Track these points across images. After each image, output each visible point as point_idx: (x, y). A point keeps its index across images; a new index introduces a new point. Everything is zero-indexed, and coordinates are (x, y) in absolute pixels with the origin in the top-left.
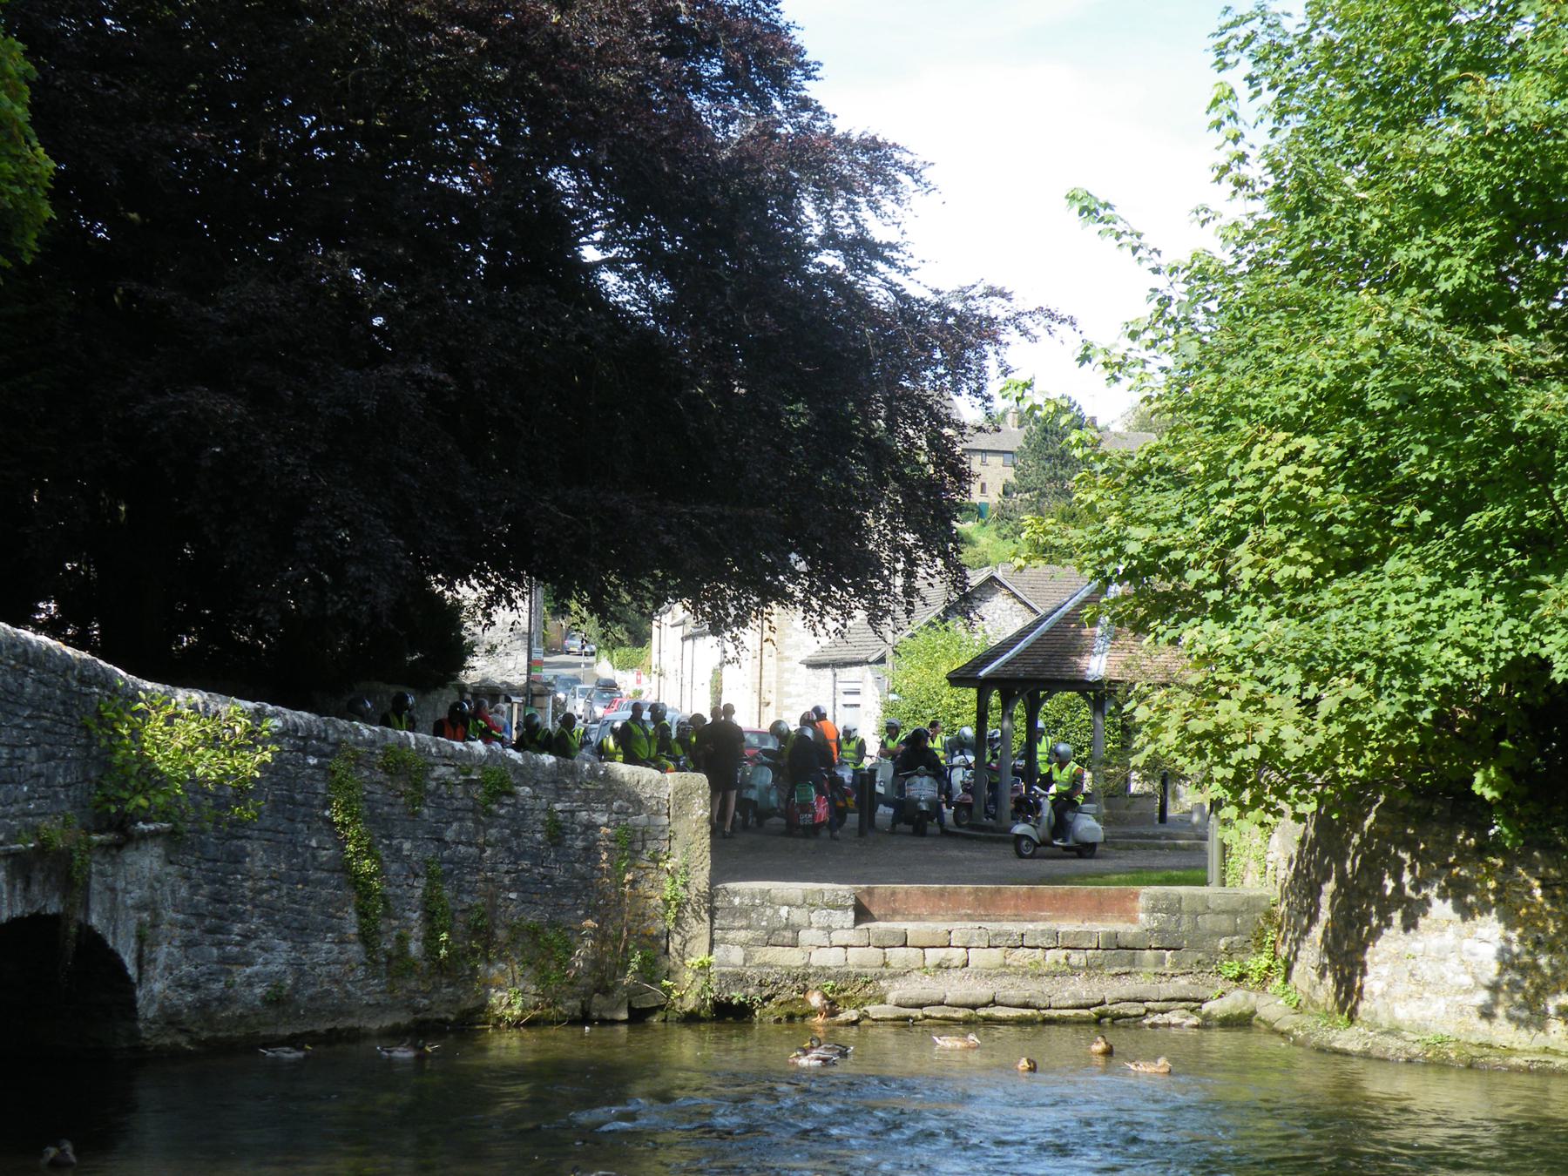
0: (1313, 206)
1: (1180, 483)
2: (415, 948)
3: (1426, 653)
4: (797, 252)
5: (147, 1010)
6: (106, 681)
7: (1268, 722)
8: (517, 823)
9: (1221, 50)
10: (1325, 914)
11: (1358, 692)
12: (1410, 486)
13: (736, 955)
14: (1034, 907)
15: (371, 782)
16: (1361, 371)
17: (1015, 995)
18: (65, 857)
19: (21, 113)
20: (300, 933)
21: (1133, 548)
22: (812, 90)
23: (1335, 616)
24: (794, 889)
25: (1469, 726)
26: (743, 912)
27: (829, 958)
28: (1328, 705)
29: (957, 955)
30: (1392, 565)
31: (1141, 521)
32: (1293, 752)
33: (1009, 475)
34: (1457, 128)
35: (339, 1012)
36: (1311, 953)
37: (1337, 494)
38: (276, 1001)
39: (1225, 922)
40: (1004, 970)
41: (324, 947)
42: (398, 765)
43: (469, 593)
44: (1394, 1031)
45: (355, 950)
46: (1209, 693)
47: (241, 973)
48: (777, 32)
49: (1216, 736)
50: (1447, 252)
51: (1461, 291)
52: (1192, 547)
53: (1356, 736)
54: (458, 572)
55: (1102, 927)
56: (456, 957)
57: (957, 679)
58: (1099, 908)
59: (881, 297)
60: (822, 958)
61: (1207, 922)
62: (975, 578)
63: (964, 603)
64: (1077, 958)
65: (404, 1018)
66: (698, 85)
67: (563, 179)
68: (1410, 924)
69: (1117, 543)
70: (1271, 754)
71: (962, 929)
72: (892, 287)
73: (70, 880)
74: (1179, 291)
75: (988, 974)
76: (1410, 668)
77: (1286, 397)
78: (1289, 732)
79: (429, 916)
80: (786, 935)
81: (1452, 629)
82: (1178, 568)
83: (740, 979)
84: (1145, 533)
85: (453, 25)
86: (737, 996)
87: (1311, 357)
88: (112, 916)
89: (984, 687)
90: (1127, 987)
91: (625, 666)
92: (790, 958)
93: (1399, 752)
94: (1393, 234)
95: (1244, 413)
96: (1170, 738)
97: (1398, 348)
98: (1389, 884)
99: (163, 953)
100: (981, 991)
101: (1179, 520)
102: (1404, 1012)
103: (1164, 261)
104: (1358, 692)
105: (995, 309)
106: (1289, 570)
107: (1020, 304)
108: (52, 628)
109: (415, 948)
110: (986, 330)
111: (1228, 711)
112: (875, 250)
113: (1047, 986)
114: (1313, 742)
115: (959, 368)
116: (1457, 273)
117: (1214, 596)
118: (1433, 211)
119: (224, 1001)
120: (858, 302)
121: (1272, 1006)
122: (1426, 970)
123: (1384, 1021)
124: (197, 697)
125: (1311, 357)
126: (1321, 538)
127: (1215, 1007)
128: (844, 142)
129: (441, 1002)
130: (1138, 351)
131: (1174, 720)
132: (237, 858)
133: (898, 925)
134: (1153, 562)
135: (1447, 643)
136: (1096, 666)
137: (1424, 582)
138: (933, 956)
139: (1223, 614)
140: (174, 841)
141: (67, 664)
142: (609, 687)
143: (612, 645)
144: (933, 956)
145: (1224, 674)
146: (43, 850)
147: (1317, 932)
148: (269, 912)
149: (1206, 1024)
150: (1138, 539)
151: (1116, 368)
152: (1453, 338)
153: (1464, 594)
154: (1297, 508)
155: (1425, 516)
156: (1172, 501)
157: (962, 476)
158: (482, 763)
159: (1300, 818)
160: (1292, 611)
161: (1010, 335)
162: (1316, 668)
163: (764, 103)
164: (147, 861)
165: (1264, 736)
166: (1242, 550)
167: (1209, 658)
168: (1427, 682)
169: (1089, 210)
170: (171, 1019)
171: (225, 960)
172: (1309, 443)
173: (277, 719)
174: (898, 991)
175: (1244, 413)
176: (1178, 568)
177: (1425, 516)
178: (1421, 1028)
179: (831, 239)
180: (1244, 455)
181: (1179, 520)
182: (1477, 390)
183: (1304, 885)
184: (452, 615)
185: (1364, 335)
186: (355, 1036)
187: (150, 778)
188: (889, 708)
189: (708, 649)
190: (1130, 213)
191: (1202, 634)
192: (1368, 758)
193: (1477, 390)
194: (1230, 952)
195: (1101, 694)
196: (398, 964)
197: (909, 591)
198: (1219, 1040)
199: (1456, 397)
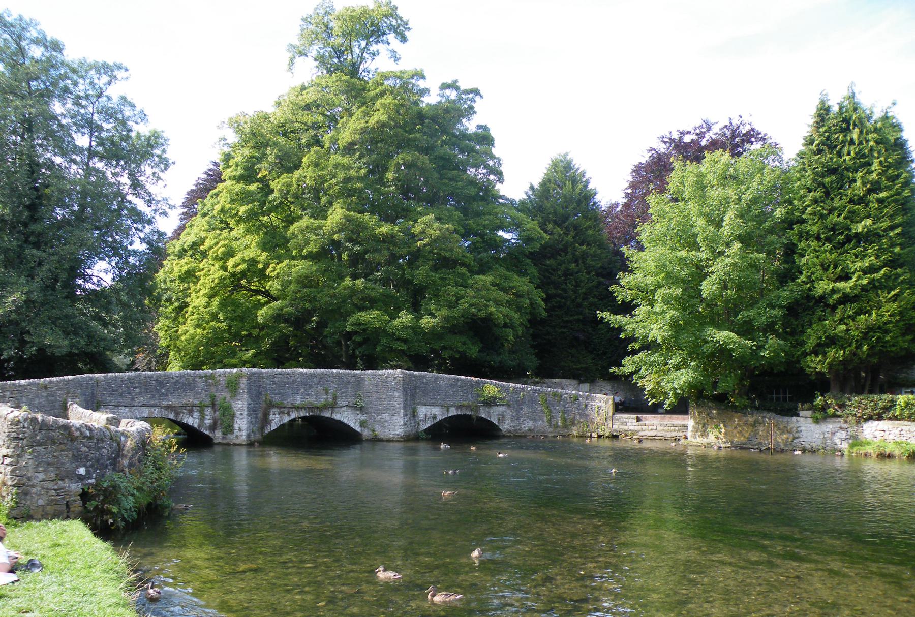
8: (579, 404)
20: (535, 420)
27: (632, 428)
29: (655, 428)
38: (529, 430)
40: (663, 430)
41: (540, 423)
47: (523, 426)
64: (677, 429)
92: (625, 428)
138: (650, 428)
144: (650, 428)
148: (528, 417)
174: (641, 433)
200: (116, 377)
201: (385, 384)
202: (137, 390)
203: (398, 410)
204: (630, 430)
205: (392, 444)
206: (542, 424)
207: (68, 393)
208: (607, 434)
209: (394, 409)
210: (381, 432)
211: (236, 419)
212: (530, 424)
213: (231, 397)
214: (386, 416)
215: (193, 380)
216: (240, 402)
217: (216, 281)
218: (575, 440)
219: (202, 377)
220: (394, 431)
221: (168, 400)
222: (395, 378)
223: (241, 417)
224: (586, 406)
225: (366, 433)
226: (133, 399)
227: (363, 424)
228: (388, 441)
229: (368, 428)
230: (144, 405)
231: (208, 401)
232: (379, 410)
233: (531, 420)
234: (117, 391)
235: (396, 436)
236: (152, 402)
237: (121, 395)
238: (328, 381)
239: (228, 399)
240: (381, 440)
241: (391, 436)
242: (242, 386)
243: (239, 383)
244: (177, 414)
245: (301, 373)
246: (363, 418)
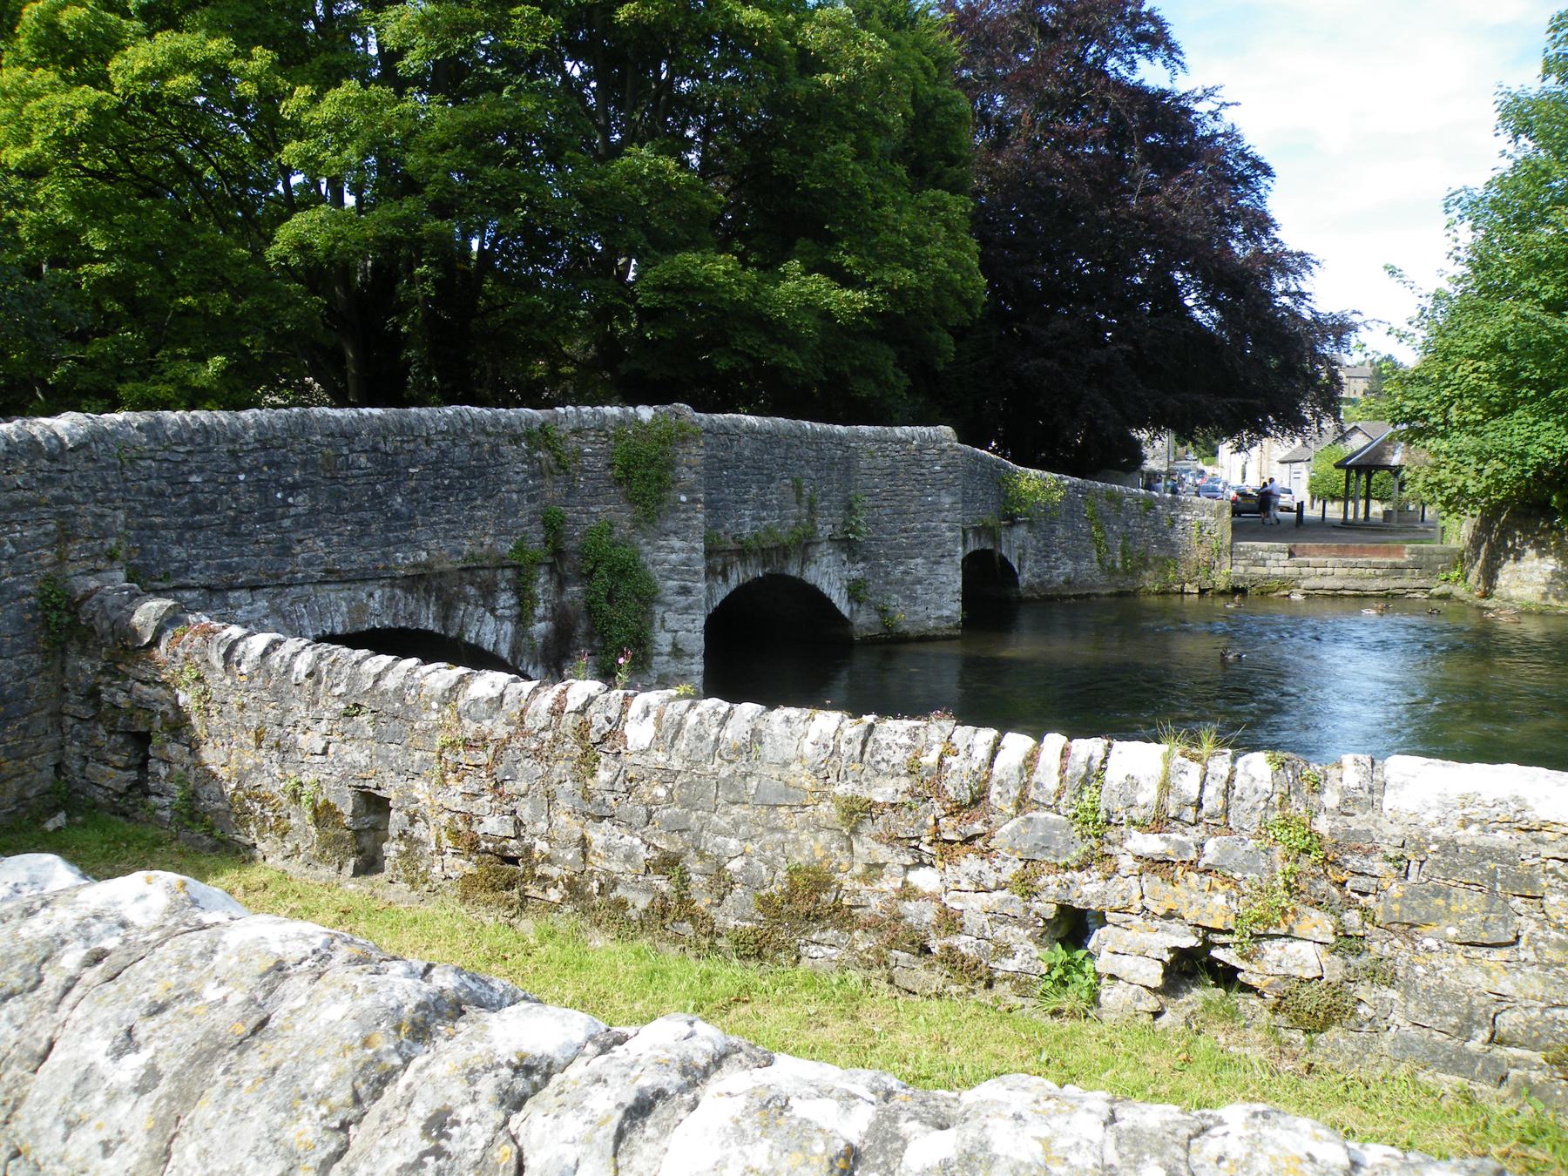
0: (1485, 267)
1: (1427, 383)
2: (1118, 565)
3: (1531, 449)
4: (1269, 297)
5: (1022, 584)
6: (1005, 467)
7: (1461, 478)
8: (1157, 519)
9: (1447, 205)
10: (1482, 556)
11: (1501, 466)
12: (1527, 380)
13: (1241, 570)
14: (1362, 551)
15: (1102, 503)
16: (1505, 334)
17: (1352, 586)
18: (991, 529)
19: (975, 264)
20: (1076, 558)
21: (1407, 410)
22: (1278, 235)
23: (1491, 435)
24: (1265, 545)
25: (1550, 479)
26: (1244, 553)
27: (1278, 571)
28: (1488, 471)
29: (1329, 570)
30: (1517, 413)
31: (1412, 399)
32: (1472, 490)
33: (1366, 386)
34: (1551, 231)
35: (1091, 587)
36: (1474, 574)
37: (1494, 385)
38: (1068, 582)
39: (1441, 558)
40: (1349, 576)
41: (1085, 564)
42: (1112, 498)
43: (1144, 435)
44: (1510, 600)
45: (1096, 565)
46: (1438, 467)
47: (1055, 572)
48: (1264, 213)
49: (1439, 484)
50: (1545, 282)
51: (1552, 298)
52: (1433, 408)
53: (1499, 484)
54: (1140, 426)
55: (1389, 560)
56: (1134, 568)
57: (1337, 466)
58: (1389, 552)
59: (1307, 315)
60: (1274, 571)
61: (1434, 558)
62: (1348, 428)
63: (1343, 436)
64: (1378, 572)
65: (1114, 590)
66: (1233, 236)
67: (1178, 276)
68: (1517, 559)
69: (1399, 407)
70: (1462, 491)
71: (1331, 561)
72: (1311, 309)
73: (995, 539)
74: (1429, 304)
75: (1342, 578)
76: (1523, 455)
77: (1472, 346)
78: (1470, 482)
79: (1124, 553)
80: (1261, 562)
81: (1543, 439)
82: (1426, 417)
83: (1242, 579)
84: (1412, 403)
85: (690, 94)
86: (1241, 585)
87: (1486, 329)
88: (1009, 549)
89: (1349, 469)
90: (1399, 583)
91: (1208, 464)
92: (1262, 571)
93: (1519, 488)
94: (1522, 276)
95: (1455, 353)
96: (1420, 485)
97: (1521, 324)
98: (1510, 544)
99: (1027, 564)
100: (1339, 584)
101: (1427, 398)
102: (1514, 593)
103: (1423, 293)
104: (1501, 466)
105: (1355, 319)
106: (1472, 417)
107: (1366, 317)
108: (994, 451)
109: (1118, 565)
110: (1352, 328)
111: (1444, 474)
112: (1303, 295)
113: (1366, 583)
114: (1481, 486)
115: (1339, 342)
116: (1550, 291)
117: (1441, 428)
118: (1539, 266)
119: (1049, 582)
120: (1297, 316)
121: (1459, 590)
122: (1525, 576)
123: (1506, 596)
124: (1038, 472)
125: (1486, 329)
126: (1486, 403)
127: (1435, 591)
128: (1290, 254)
129: (1127, 584)
130: (1412, 329)
131: (1421, 478)
132: (1053, 531)
133: (1306, 559)
134: (1415, 415)
135: (1540, 445)
136: (1395, 460)
137: (1531, 420)
138: (1320, 571)
139: (1444, 436)
140: (1031, 524)
141: (992, 461)
142: (1202, 472)
143: (1202, 457)
144: (1320, 571)
145: (1442, 458)
146: (984, 527)
147: (1480, 562)
148: (1065, 550)
149: (1431, 597)
150: (1409, 406)
151: (1402, 337)
152: (1546, 318)
153: (1549, 424)
154: (1474, 391)
155: (1533, 392)
156: (1425, 390)
157: (1340, 386)
158: (1143, 497)
159: (1473, 516)
160: (1474, 433)
161: (1361, 328)
162: (1484, 458)
163: (1257, 239)
164: (1021, 531)
165: (1459, 484)
166: (1452, 409)
167: (1437, 453)
168: (1530, 461)
169: (1392, 273)
170: (1031, 587)
171: (1050, 567)
172: (1483, 364)
173: (1068, 480)
174: (1306, 584)
175: (1455, 353)
176: (1426, 417)
177: (1533, 392)
178: (1520, 599)
179: (1285, 293)
180: (1455, 370)
181: (1427, 398)
182: (1557, 338)
183: (1476, 542)
184: (1138, 444)
185: (1507, 319)
186: (1097, 595)
187: (1021, 502)
188: (1312, 478)
189: (1240, 458)
190: (1409, 274)
191: (1434, 443)
192: (1503, 492)
193: (1557, 338)
194: (1443, 570)
195: (1396, 471)
196: (1112, 571)
197: (1320, 430)
198: (1436, 604)
199: (1547, 341)
200: (206, 431)
201: (915, 469)
202: (301, 502)
203: (950, 546)
204: (1275, 577)
205: (931, 649)
206: (1088, 568)
207: (66, 535)
208: (1222, 587)
209: (939, 545)
210: (908, 616)
211: (659, 610)
212: (1067, 568)
213: (636, 524)
214: (918, 565)
215: (495, 451)
216: (676, 543)
217: (83, 116)
218: (1154, 600)
219: (515, 439)
220: (940, 608)
221: (416, 545)
222: (943, 451)
223: (682, 601)
224: (1173, 522)
225: (863, 620)
226: (285, 551)
227: (855, 592)
228: (924, 639)
229: (869, 604)
230: (333, 577)
231: (536, 541)
232: (900, 547)
233: (1071, 557)
234: (211, 508)
235: (944, 625)
236: (360, 558)
237: (234, 530)
238: (800, 458)
239: (624, 528)
240: (904, 639)
241: (931, 623)
242: (688, 476)
243: (671, 466)
244: (447, 610)
245: (751, 430)
246: (854, 574)
